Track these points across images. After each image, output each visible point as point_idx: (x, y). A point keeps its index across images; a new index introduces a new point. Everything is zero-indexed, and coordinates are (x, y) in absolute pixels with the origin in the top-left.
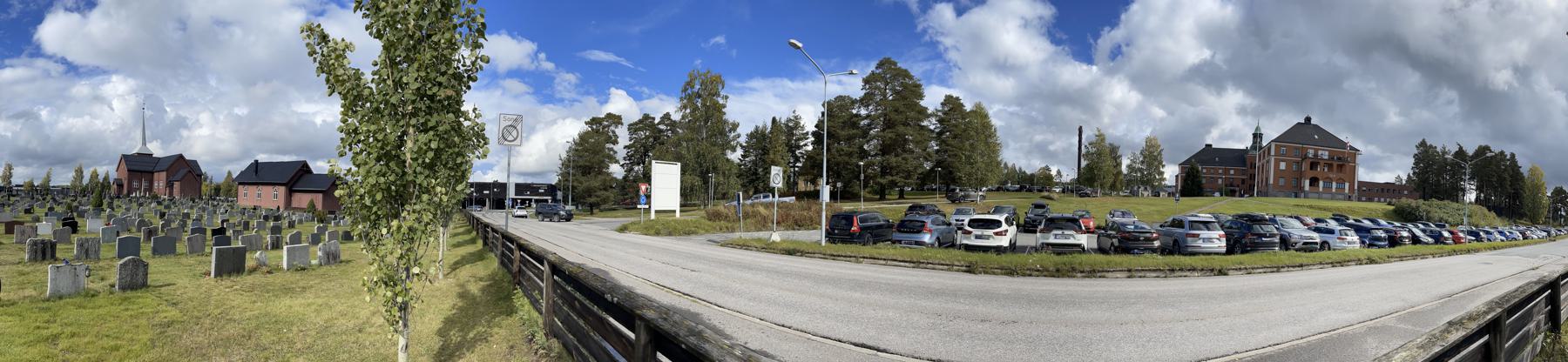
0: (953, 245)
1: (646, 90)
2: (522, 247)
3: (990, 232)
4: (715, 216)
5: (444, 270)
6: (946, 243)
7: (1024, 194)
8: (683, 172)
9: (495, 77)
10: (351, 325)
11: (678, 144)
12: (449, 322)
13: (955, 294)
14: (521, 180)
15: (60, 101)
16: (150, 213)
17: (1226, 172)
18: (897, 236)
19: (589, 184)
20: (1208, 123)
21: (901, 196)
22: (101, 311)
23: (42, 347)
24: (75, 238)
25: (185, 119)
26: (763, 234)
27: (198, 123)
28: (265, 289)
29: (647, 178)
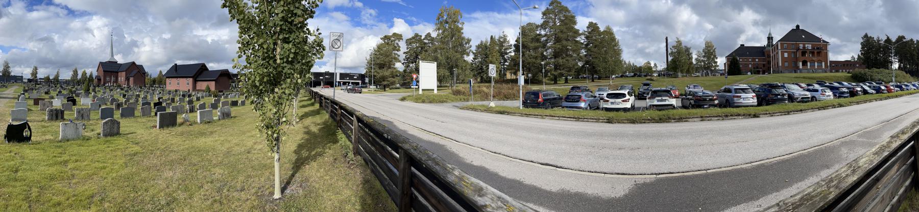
0: (598, 108)
1: (414, 19)
2: (342, 108)
3: (620, 100)
4: (457, 93)
5: (298, 120)
6: (594, 107)
7: (636, 78)
8: (438, 67)
9: (326, 11)
10: (243, 150)
11: (435, 51)
12: (300, 147)
13: (601, 135)
14: (343, 71)
15: (64, 31)
16: (118, 95)
17: (754, 60)
18: (565, 104)
19: (381, 73)
20: (739, 31)
21: (566, 81)
22: (93, 148)
23: (58, 167)
24: (75, 108)
25: (136, 41)
26: (485, 103)
27: (143, 44)
28: (190, 134)
29: (417, 70)
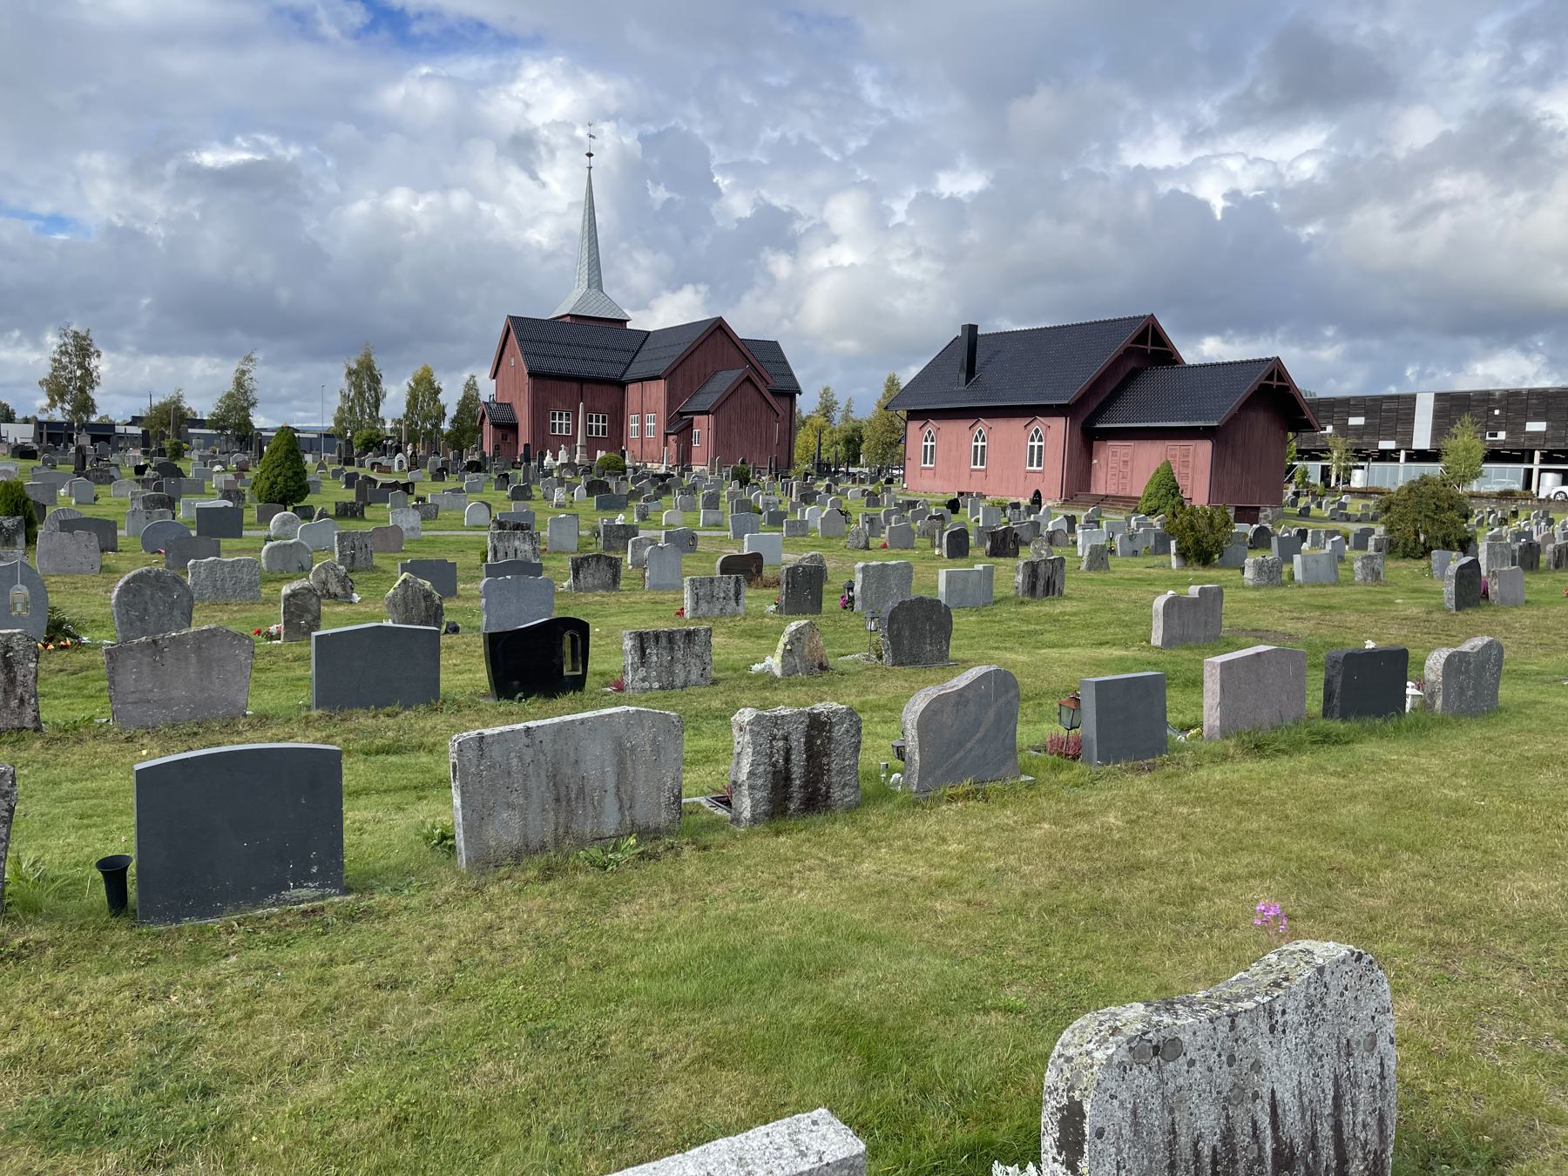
25: (790, 216)
